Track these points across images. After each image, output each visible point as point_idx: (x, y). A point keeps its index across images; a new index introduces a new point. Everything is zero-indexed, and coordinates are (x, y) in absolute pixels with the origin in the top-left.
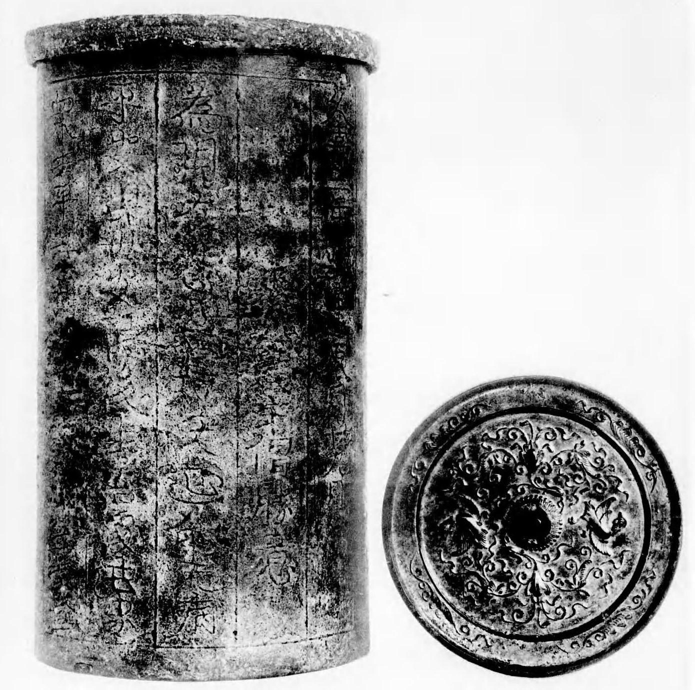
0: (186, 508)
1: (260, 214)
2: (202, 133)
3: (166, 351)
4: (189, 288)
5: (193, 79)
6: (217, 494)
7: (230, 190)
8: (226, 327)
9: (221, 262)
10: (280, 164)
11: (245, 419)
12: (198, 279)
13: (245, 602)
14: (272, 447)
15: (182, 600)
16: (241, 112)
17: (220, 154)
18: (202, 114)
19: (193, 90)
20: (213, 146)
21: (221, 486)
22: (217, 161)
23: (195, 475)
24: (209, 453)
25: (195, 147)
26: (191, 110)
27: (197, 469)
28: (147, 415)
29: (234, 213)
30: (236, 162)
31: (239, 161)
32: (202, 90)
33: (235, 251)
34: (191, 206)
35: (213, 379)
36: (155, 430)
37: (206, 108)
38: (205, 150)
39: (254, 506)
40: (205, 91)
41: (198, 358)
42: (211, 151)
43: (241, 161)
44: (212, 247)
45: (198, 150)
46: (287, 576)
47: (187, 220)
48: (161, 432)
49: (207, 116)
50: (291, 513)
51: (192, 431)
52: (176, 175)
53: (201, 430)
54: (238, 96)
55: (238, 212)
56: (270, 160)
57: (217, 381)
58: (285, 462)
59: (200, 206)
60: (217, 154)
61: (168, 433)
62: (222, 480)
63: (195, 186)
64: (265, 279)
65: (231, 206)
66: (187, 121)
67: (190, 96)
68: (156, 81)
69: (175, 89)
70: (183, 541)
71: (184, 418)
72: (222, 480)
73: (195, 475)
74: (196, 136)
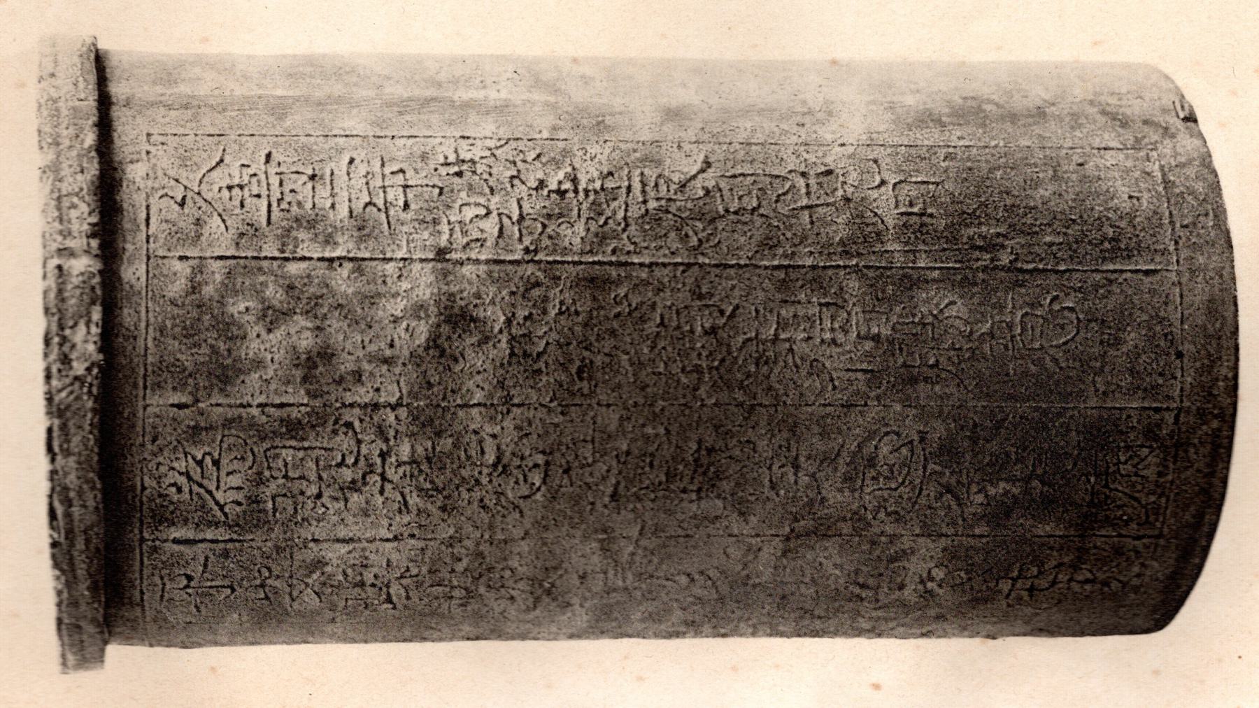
0: (932, 490)
1: (404, 364)
2: (254, 470)
3: (650, 523)
4: (539, 489)
5: (154, 484)
6: (911, 442)
7: (361, 421)
8: (613, 427)
9: (494, 436)
10: (310, 325)
11: (782, 392)
12: (525, 476)
13: (1104, 393)
14: (834, 342)
15: (1088, 498)
16: (213, 402)
17: (293, 438)
18: (218, 469)
19: (174, 485)
20: (277, 451)
21: (898, 434)
22: (306, 444)
23: (873, 478)
24: (838, 455)
25: (281, 481)
26: (212, 487)
27: (864, 474)
28: (760, 550)
29: (403, 413)
30: (308, 409)
31: (306, 405)
32: (173, 469)
33: (475, 412)
34: (388, 487)
35: (707, 449)
36: (788, 539)
37: (208, 460)
38: (286, 465)
39: (938, 376)
40: (176, 465)
41: (667, 474)
42: (287, 454)
43: (305, 401)
44: (466, 451)
45: (286, 477)
46: (1066, 313)
47: (414, 494)
48: (792, 530)
49: (224, 462)
50: (953, 303)
51: (796, 482)
52: (331, 511)
53: (796, 467)
54: (180, 406)
55: (402, 405)
56: (304, 343)
57: (709, 440)
58: (861, 315)
59: (390, 473)
60: (293, 443)
61: (796, 520)
62: (887, 434)
63: (353, 482)
64: (526, 355)
65: (392, 418)
66: (232, 495)
67: (186, 489)
68: (157, 543)
69: (172, 513)
70: (987, 496)
71: (772, 494)
72: (887, 434)
73: (873, 478)
74: (259, 481)
